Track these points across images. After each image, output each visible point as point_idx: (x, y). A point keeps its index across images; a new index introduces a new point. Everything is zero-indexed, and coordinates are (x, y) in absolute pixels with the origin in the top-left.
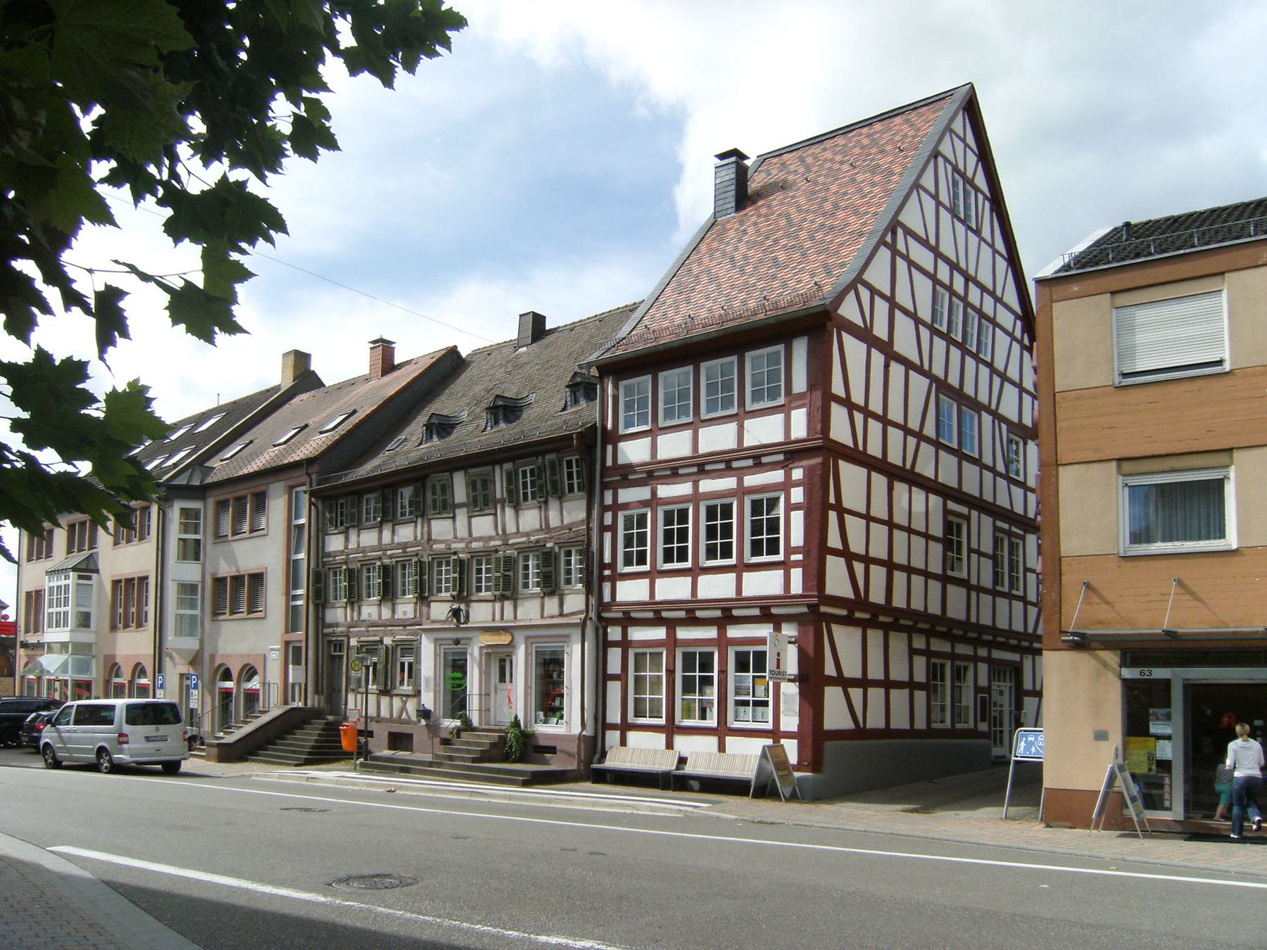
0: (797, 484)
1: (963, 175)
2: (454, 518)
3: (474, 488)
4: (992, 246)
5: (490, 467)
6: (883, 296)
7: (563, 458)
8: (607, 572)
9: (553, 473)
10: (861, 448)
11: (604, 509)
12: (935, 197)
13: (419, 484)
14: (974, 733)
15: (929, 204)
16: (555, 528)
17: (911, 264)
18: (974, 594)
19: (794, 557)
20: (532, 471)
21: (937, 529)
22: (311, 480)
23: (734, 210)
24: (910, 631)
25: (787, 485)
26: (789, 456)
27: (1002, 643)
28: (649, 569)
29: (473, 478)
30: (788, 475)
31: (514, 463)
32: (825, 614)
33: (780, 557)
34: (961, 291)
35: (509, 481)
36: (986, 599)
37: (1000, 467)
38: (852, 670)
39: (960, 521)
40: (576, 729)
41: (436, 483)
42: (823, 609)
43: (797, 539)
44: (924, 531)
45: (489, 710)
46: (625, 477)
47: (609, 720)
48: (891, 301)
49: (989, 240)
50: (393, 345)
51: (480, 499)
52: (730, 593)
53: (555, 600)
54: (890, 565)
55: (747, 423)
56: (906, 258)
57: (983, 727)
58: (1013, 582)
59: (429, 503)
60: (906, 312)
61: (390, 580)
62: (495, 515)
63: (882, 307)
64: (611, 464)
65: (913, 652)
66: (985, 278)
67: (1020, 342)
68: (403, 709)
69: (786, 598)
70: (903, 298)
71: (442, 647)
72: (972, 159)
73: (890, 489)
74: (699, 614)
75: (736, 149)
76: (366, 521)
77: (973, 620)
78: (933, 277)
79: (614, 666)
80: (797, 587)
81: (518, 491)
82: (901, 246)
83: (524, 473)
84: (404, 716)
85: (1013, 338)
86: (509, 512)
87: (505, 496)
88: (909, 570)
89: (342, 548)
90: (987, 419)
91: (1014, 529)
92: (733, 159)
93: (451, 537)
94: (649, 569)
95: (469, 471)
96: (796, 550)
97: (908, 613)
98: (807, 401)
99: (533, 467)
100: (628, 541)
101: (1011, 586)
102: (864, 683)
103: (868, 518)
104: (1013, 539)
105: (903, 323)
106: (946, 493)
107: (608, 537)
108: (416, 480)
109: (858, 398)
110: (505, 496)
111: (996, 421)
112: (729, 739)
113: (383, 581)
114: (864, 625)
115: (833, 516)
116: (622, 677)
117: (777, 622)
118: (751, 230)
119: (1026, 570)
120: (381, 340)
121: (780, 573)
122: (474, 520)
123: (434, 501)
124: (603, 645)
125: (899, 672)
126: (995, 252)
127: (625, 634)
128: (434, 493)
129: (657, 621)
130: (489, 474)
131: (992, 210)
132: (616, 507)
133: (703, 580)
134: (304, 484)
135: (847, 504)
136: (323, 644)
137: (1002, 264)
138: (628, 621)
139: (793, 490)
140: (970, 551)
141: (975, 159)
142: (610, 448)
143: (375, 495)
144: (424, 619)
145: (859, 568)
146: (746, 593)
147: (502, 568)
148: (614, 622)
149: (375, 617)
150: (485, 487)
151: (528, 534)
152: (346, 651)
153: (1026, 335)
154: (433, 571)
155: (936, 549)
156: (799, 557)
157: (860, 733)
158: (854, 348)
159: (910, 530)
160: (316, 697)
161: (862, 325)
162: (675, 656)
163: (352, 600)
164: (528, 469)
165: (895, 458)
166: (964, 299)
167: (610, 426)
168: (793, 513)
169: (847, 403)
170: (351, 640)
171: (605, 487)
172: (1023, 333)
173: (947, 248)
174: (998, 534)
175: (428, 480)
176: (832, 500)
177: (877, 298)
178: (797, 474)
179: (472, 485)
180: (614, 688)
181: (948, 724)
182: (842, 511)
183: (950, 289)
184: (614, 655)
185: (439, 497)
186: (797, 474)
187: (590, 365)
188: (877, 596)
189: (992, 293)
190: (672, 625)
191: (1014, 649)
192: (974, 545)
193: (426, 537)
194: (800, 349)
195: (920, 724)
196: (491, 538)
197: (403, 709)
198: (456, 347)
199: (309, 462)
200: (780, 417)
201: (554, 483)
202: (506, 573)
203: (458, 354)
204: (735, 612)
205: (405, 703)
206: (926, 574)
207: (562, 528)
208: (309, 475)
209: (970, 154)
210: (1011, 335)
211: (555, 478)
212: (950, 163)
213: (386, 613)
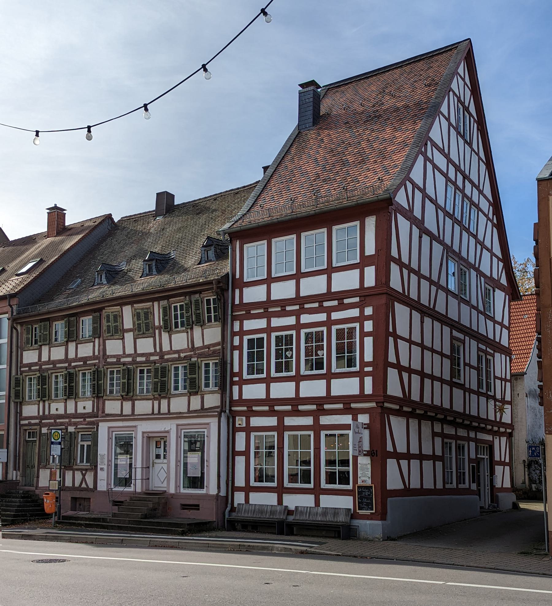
0: (368, 318)
1: (463, 104)
2: (123, 339)
3: (139, 318)
4: (478, 154)
5: (151, 303)
6: (419, 189)
7: (204, 297)
8: (236, 379)
9: (197, 308)
10: (406, 294)
11: (234, 334)
12: (448, 119)
13: (97, 314)
14: (468, 491)
15: (444, 123)
16: (197, 348)
17: (435, 167)
18: (467, 394)
19: (366, 369)
20: (181, 306)
21: (447, 350)
22: (12, 309)
23: (311, 124)
24: (433, 419)
25: (361, 319)
26: (363, 299)
27: (483, 428)
28: (265, 376)
29: (138, 311)
30: (362, 312)
31: (168, 300)
32: (387, 408)
33: (357, 368)
34: (461, 186)
35: (165, 314)
36: (474, 397)
37: (481, 308)
38: (401, 448)
39: (459, 344)
40: (213, 491)
41: (110, 313)
42: (386, 405)
43: (369, 357)
44: (440, 351)
45: (148, 479)
46: (248, 312)
47: (237, 484)
48: (423, 191)
49: (476, 151)
50: (64, 212)
51: (143, 327)
52: (323, 393)
53: (199, 397)
54: (422, 374)
55: (334, 275)
56: (432, 162)
57: (474, 487)
58: (488, 388)
59: (105, 328)
60: (431, 200)
61: (74, 384)
62: (154, 337)
63: (418, 195)
64: (238, 303)
65: (434, 434)
66: (474, 177)
67: (492, 221)
68: (84, 479)
69: (362, 397)
70: (430, 191)
71: (183, 431)
72: (468, 93)
73: (422, 322)
74: (301, 408)
75: (313, 81)
76: (55, 341)
77: (467, 412)
78: (445, 175)
79: (240, 446)
80: (369, 390)
81: (171, 321)
82: (429, 154)
83: (176, 308)
84: (84, 485)
85: (488, 219)
86: (165, 336)
87: (161, 324)
88: (432, 378)
89: (36, 360)
90: (473, 273)
91: (488, 349)
92: (312, 88)
93: (121, 353)
94: (265, 376)
95: (135, 305)
96: (368, 364)
97: (432, 407)
98: (376, 261)
99: (182, 303)
100: (251, 356)
101: (487, 390)
102: (408, 456)
103: (410, 342)
104: (488, 357)
105: (430, 207)
106: (455, 325)
107: (236, 353)
108: (95, 311)
109: (405, 260)
110: (161, 324)
111: (478, 275)
112: (322, 497)
113: (69, 385)
114: (408, 416)
115: (391, 339)
116: (246, 453)
117: (355, 413)
118: (325, 140)
119: (495, 377)
120: (56, 207)
121: (324, 382)
122: (138, 340)
123: (108, 327)
124: (233, 430)
125: (427, 450)
126: (480, 159)
127: (248, 422)
128: (108, 321)
129: (271, 413)
130: (149, 308)
131: (478, 129)
132: (242, 333)
133: (303, 385)
134: (7, 313)
135: (398, 332)
136: (20, 432)
137: (483, 167)
138: (250, 414)
139: (366, 323)
140: (465, 364)
141: (470, 93)
142: (237, 292)
143: (63, 322)
144: (100, 412)
145: (405, 375)
146: (334, 393)
147: (159, 376)
148: (241, 413)
149: (61, 411)
150: (146, 318)
151: (178, 352)
152: (38, 437)
153: (495, 216)
154: (107, 378)
155: (447, 363)
156: (370, 369)
157: (407, 491)
158: (403, 224)
159: (433, 351)
160: (14, 472)
161: (407, 208)
162: (283, 437)
163: (44, 399)
164: (178, 305)
165: (424, 301)
166: (462, 191)
167: (238, 276)
168: (366, 339)
169: (399, 262)
170: (43, 429)
171: (234, 318)
172: (493, 215)
173: (454, 156)
174: (480, 353)
175: (104, 311)
176: (391, 330)
177: (416, 190)
178: (369, 311)
179: (137, 315)
180: (240, 461)
181: (454, 485)
182: (397, 337)
183: (455, 184)
184: (241, 438)
185: (112, 324)
186: (369, 311)
187: (224, 232)
188: (415, 396)
189: (478, 188)
190: (281, 416)
191: (490, 432)
192: (467, 361)
193: (101, 353)
194: (371, 222)
195: (440, 485)
196: (152, 354)
197: (84, 479)
198: (111, 215)
199: (11, 296)
200: (357, 272)
201: (198, 316)
202: (163, 379)
203: (112, 219)
204: (326, 407)
205: (84, 475)
206: (441, 380)
207: (204, 347)
208: (11, 306)
209: (467, 90)
210: (486, 216)
211: (198, 311)
212: (456, 96)
213: (71, 409)
